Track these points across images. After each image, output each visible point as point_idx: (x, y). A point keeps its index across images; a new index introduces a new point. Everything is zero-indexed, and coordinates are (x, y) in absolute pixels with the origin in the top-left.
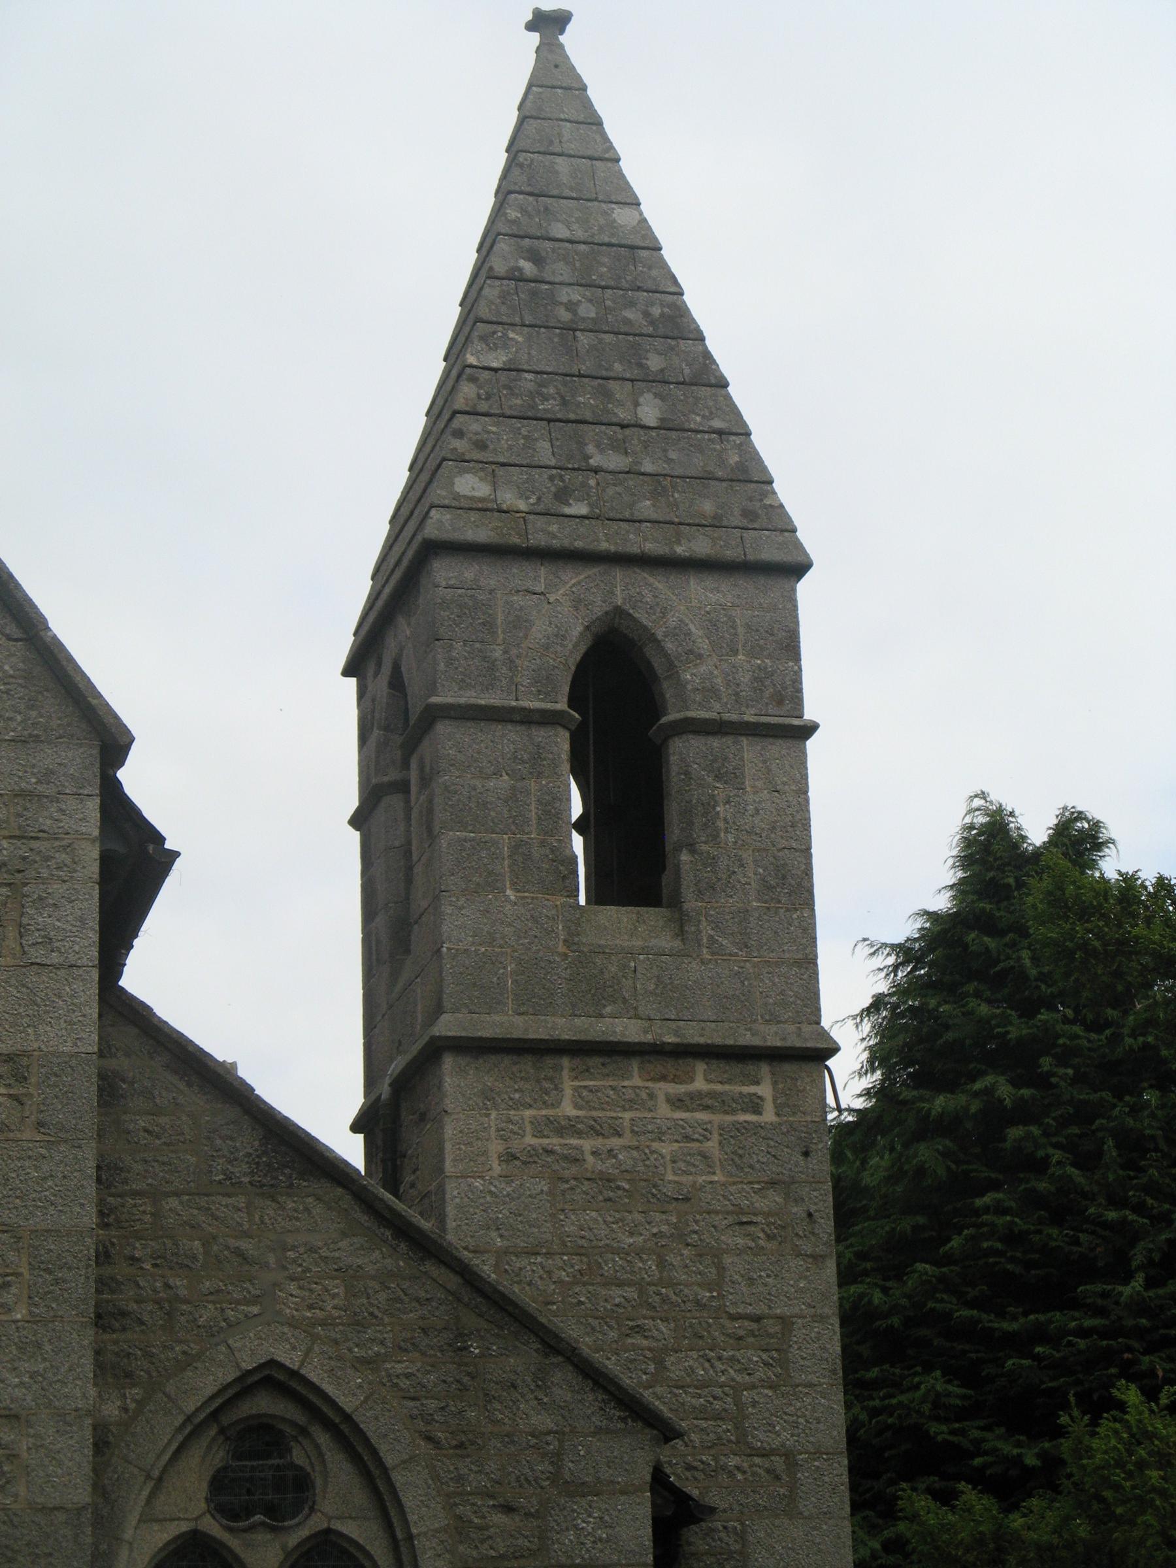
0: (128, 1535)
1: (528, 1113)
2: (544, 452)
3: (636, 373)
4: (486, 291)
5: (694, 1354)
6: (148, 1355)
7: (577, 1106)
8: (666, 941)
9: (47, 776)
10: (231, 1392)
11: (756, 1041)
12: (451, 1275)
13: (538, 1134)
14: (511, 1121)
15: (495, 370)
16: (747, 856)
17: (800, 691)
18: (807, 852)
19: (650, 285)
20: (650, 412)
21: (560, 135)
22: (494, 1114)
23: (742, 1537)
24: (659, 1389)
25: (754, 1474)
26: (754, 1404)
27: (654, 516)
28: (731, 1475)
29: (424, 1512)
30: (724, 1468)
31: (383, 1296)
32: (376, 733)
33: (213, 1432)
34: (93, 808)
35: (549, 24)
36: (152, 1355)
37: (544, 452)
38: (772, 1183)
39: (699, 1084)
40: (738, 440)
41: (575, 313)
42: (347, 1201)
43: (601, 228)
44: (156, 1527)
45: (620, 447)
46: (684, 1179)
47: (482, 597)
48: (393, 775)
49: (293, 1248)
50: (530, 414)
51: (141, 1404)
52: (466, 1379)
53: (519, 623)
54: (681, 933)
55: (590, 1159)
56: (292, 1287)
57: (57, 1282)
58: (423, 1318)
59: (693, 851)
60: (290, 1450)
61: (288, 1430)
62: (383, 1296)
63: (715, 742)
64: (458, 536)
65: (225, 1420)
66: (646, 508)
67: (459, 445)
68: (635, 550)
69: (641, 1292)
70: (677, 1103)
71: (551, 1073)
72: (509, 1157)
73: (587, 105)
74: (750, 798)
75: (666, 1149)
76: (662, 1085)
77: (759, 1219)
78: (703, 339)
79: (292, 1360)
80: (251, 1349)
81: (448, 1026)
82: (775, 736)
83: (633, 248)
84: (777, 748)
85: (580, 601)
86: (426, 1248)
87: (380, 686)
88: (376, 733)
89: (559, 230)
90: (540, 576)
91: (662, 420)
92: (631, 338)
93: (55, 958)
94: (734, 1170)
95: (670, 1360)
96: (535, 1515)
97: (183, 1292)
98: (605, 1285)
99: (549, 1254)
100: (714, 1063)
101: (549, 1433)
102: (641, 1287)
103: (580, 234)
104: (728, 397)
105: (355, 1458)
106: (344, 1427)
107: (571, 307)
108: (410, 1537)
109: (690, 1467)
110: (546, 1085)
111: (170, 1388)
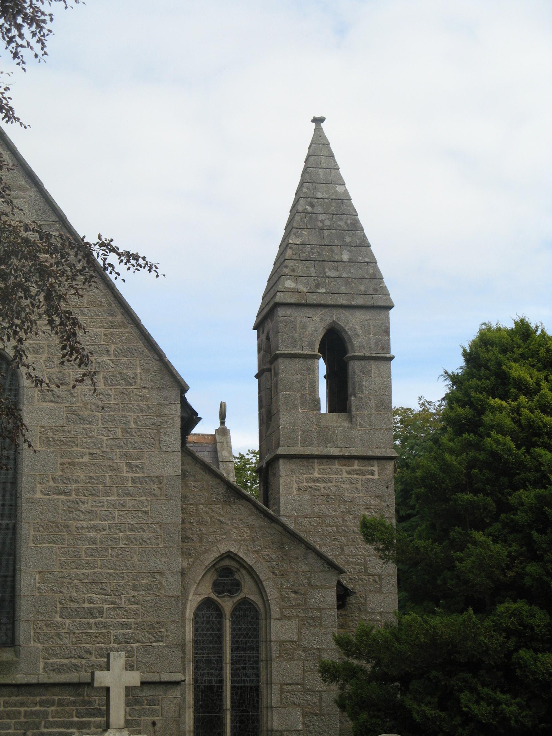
0: (190, 598)
1: (305, 476)
2: (312, 272)
3: (342, 243)
4: (296, 217)
5: (352, 546)
6: (195, 549)
7: (319, 474)
8: (346, 424)
9: (166, 399)
10: (218, 559)
11: (373, 454)
12: (280, 527)
13: (308, 482)
14: (299, 479)
15: (298, 244)
16: (372, 397)
17: (389, 345)
18: (390, 396)
19: (347, 213)
20: (345, 257)
21: (321, 161)
22: (294, 476)
23: (365, 599)
24: (342, 557)
25: (369, 581)
26: (370, 561)
27: (346, 292)
28: (362, 581)
29: (272, 593)
30: (361, 579)
31: (260, 533)
32: (262, 352)
33: (213, 570)
34: (179, 407)
35: (318, 121)
36: (196, 549)
37: (312, 272)
38: (377, 496)
39: (356, 467)
40: (373, 265)
41: (323, 224)
42: (251, 506)
43: (333, 194)
44: (198, 596)
45: (336, 269)
46: (350, 495)
47: (292, 319)
48: (267, 366)
49: (235, 519)
50: (308, 259)
51: (193, 562)
52: (284, 556)
53: (304, 327)
54: (351, 422)
55: (323, 489)
56: (235, 530)
57: (171, 537)
58: (272, 539)
59: (355, 396)
60: (235, 575)
61: (234, 569)
62: (260, 533)
63: (363, 362)
64: (285, 301)
65: (217, 567)
66: (343, 289)
67: (286, 270)
68: (339, 303)
69: (337, 528)
70: (349, 473)
71: (311, 464)
72: (299, 489)
73: (330, 150)
74: (373, 379)
75: (346, 486)
76: (345, 467)
77: (373, 507)
78: (363, 231)
79: (235, 551)
80: (223, 548)
81: (281, 451)
82: (382, 360)
83: (342, 200)
84: (382, 364)
85: (322, 319)
86: (272, 520)
87: (264, 337)
88: (262, 352)
89: (319, 195)
90: (310, 312)
91: (349, 259)
92: (340, 231)
93: (169, 449)
94: (365, 492)
95: (345, 548)
96: (304, 594)
97: (204, 532)
98: (327, 526)
99: (310, 517)
100: (360, 460)
101: (308, 571)
102: (337, 527)
103: (326, 196)
104: (371, 250)
105: (253, 578)
106: (250, 569)
107: (322, 221)
108: (268, 600)
109: (350, 579)
110: (310, 467)
111: (201, 558)
